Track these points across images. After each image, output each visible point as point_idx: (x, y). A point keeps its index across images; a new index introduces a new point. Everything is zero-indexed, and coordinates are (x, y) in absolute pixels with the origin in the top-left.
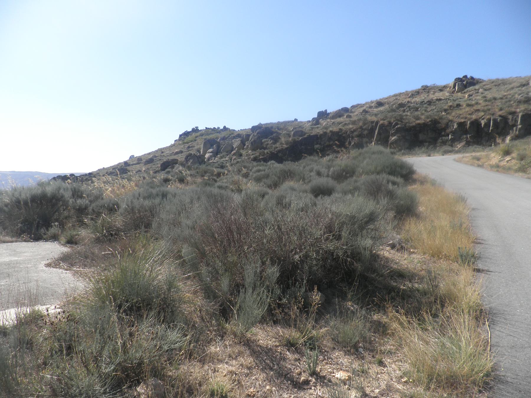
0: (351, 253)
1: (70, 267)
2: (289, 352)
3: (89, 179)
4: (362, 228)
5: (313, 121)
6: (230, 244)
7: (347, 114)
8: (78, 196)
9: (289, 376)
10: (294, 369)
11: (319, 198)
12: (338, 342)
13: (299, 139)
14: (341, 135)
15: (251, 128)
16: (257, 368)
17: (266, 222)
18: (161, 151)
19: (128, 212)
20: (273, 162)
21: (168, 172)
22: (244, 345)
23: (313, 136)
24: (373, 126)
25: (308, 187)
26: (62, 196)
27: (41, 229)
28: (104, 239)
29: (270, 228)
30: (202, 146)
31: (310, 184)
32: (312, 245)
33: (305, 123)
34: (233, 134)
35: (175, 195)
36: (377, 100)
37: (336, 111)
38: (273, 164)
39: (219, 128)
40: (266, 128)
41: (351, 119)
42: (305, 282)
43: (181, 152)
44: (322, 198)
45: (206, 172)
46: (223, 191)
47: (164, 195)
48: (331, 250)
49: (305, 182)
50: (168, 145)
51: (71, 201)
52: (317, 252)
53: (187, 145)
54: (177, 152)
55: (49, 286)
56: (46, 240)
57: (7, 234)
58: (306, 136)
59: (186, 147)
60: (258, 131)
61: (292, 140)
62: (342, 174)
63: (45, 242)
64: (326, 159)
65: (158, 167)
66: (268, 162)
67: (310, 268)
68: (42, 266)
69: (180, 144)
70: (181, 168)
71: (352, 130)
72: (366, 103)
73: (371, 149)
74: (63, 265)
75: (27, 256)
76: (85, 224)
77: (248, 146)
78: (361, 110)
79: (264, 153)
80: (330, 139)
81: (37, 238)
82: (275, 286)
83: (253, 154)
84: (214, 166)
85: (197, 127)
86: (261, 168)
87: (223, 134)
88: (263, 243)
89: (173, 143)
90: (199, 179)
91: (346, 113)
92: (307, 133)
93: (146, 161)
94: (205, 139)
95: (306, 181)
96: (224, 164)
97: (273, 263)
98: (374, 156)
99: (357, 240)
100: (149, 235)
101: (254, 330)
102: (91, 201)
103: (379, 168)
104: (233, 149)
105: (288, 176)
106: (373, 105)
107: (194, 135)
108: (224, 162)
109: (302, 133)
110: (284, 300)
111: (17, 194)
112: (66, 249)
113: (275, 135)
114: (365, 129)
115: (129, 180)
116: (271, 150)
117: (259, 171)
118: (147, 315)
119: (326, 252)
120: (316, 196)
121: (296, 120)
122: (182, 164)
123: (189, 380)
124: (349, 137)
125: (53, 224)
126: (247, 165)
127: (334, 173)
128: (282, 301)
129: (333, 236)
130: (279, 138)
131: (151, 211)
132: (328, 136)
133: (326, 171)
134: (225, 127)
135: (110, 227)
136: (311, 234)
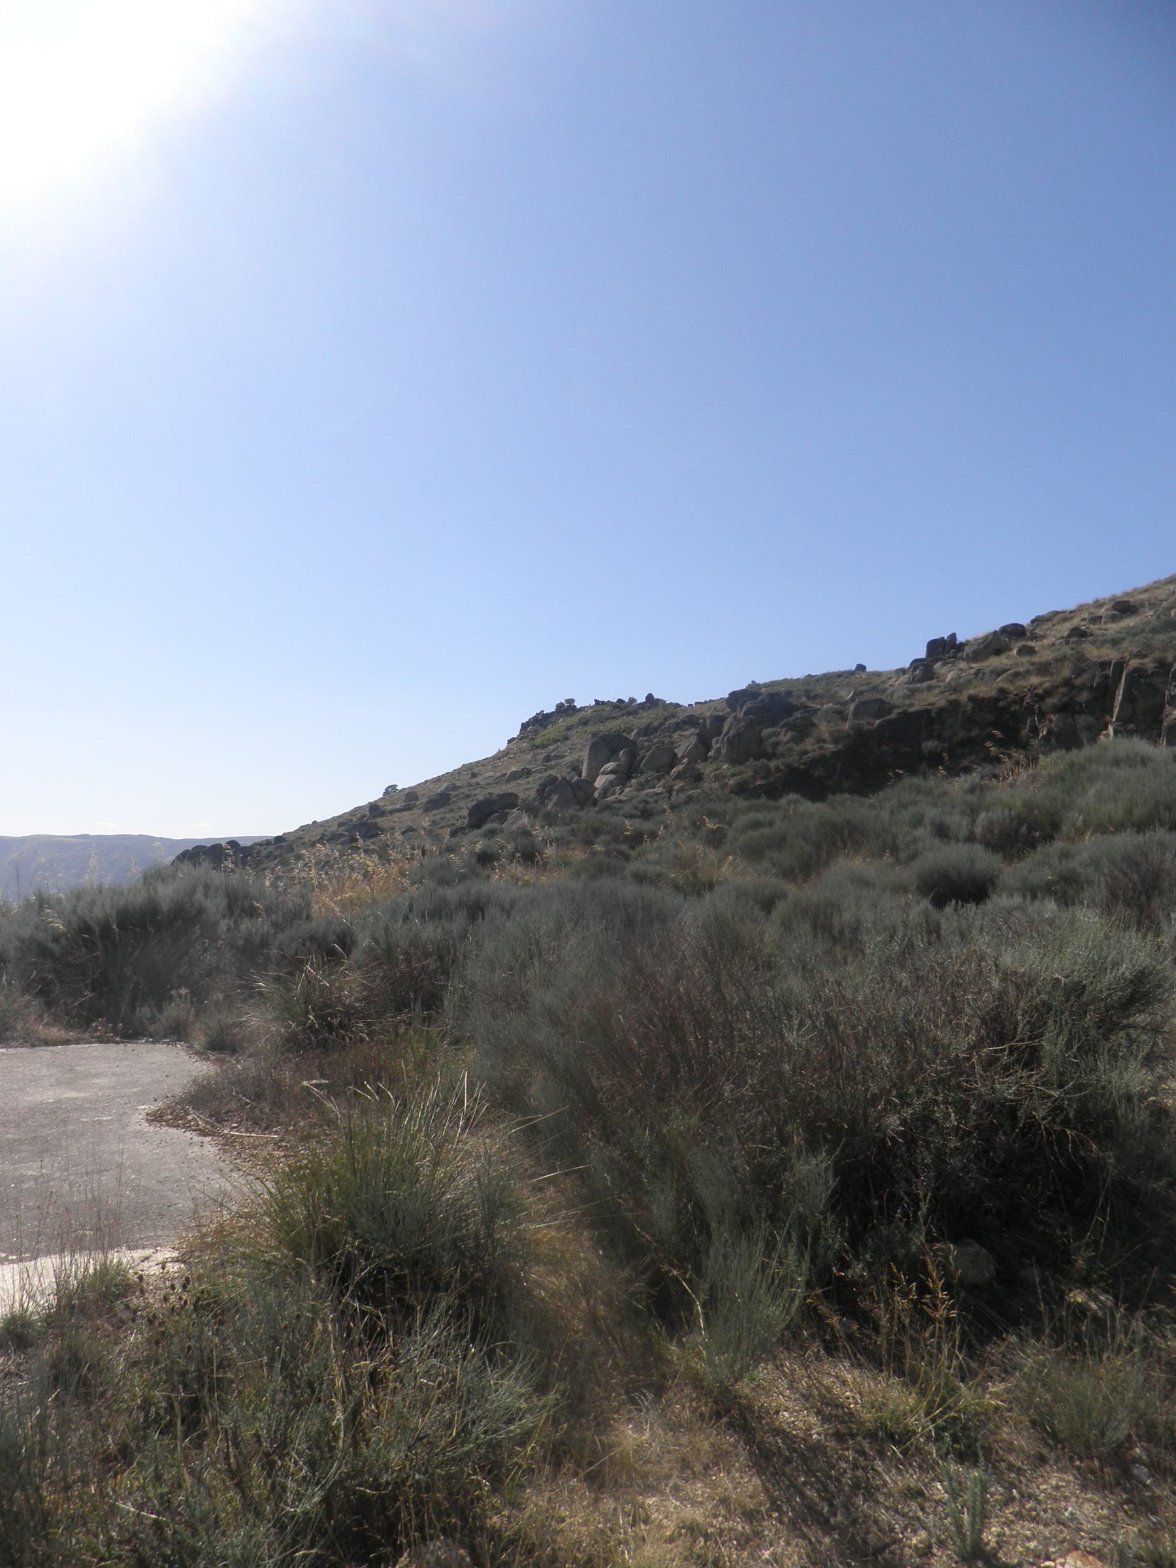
0: (1078, 1111)
1: (213, 1126)
2: (883, 1461)
3: (275, 853)
4: (1108, 1025)
5: (915, 670)
6: (675, 1072)
7: (1020, 644)
8: (243, 910)
9: (887, 1554)
10: (905, 1528)
11: (948, 909)
12: (1058, 1440)
13: (873, 724)
14: (1004, 709)
15: (727, 696)
16: (776, 1515)
17: (786, 1005)
18: (471, 770)
19: (376, 958)
20: (793, 796)
21: (492, 833)
22: (730, 1425)
23: (917, 713)
24: (1107, 676)
25: (908, 874)
26: (201, 910)
27: (142, 1005)
28: (309, 1038)
29: (801, 1025)
30: (585, 754)
31: (915, 866)
32: (941, 1082)
33: (888, 676)
34: (673, 716)
35: (507, 910)
36: (1113, 598)
37: (986, 638)
38: (796, 802)
39: (632, 700)
40: (774, 697)
41: (1036, 659)
42: (924, 1207)
43: (526, 773)
44: (956, 910)
45: (597, 832)
46: (649, 891)
47: (476, 909)
48: (1006, 1100)
49: (897, 859)
50: (491, 753)
51: (223, 925)
52: (962, 1109)
53: (542, 754)
54: (513, 773)
55: (153, 1184)
56: (156, 1038)
57: (56, 1021)
58: (893, 716)
59: (541, 757)
60: (748, 705)
61: (852, 728)
62: (1017, 831)
63: (153, 1043)
64: (962, 782)
65: (461, 817)
66: (781, 796)
67: (940, 1158)
68: (137, 1120)
69: (522, 751)
70: (525, 820)
71: (1040, 692)
72: (1081, 608)
73: (1106, 749)
74: (194, 1119)
75: (101, 1088)
76: (261, 994)
77: (719, 750)
78: (1065, 629)
79: (767, 768)
80: (969, 722)
81: (131, 1033)
82: (825, 1219)
83: (733, 775)
84: (621, 812)
85: (570, 701)
86: (760, 816)
87: (646, 718)
88: (780, 1075)
89: (503, 746)
90: (576, 852)
91: (1017, 640)
92: (895, 707)
93: (429, 802)
94: (594, 735)
95: (902, 855)
96: (649, 807)
97: (812, 1147)
98: (1122, 772)
99: (1094, 1070)
100: (434, 1030)
101: (764, 1372)
102: (275, 925)
103: (1139, 812)
104: (674, 761)
105: (843, 841)
106: (1102, 611)
107: (562, 722)
108: (650, 800)
109: (882, 707)
110: (858, 1270)
111: (82, 907)
112: (204, 1069)
113: (798, 715)
114: (1081, 688)
115: (385, 858)
116: (789, 760)
117: (756, 825)
118: (426, 1312)
119: (990, 1107)
120: (940, 902)
121: (861, 668)
122: (531, 809)
123: (553, 1549)
124: (1032, 713)
125: (173, 992)
126: (717, 806)
127: (989, 828)
128: (850, 1273)
129: (1011, 1054)
130: (813, 725)
131: (441, 958)
132: (965, 712)
133: (965, 823)
134: (650, 697)
135: (326, 1006)
136: (936, 1046)
